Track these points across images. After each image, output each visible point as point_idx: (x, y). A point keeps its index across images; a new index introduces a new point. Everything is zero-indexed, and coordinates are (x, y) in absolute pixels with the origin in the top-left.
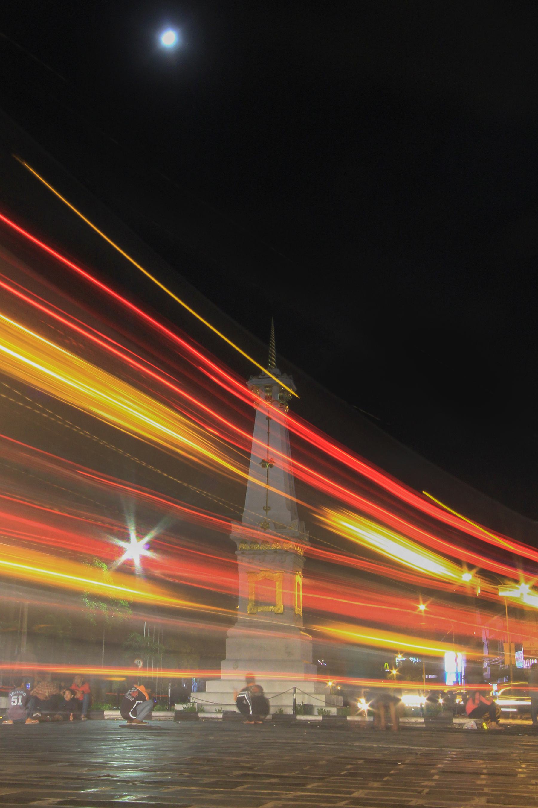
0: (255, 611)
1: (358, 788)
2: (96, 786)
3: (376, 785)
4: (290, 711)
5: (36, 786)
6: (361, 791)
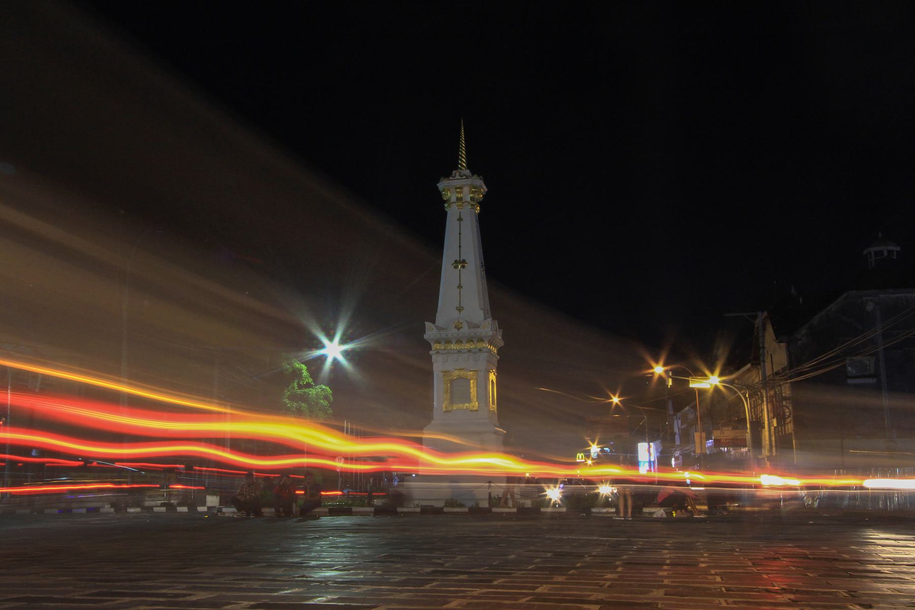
0: (450, 409)
1: (542, 583)
2: (291, 587)
3: (561, 579)
4: (485, 504)
5: (229, 589)
6: (545, 586)
